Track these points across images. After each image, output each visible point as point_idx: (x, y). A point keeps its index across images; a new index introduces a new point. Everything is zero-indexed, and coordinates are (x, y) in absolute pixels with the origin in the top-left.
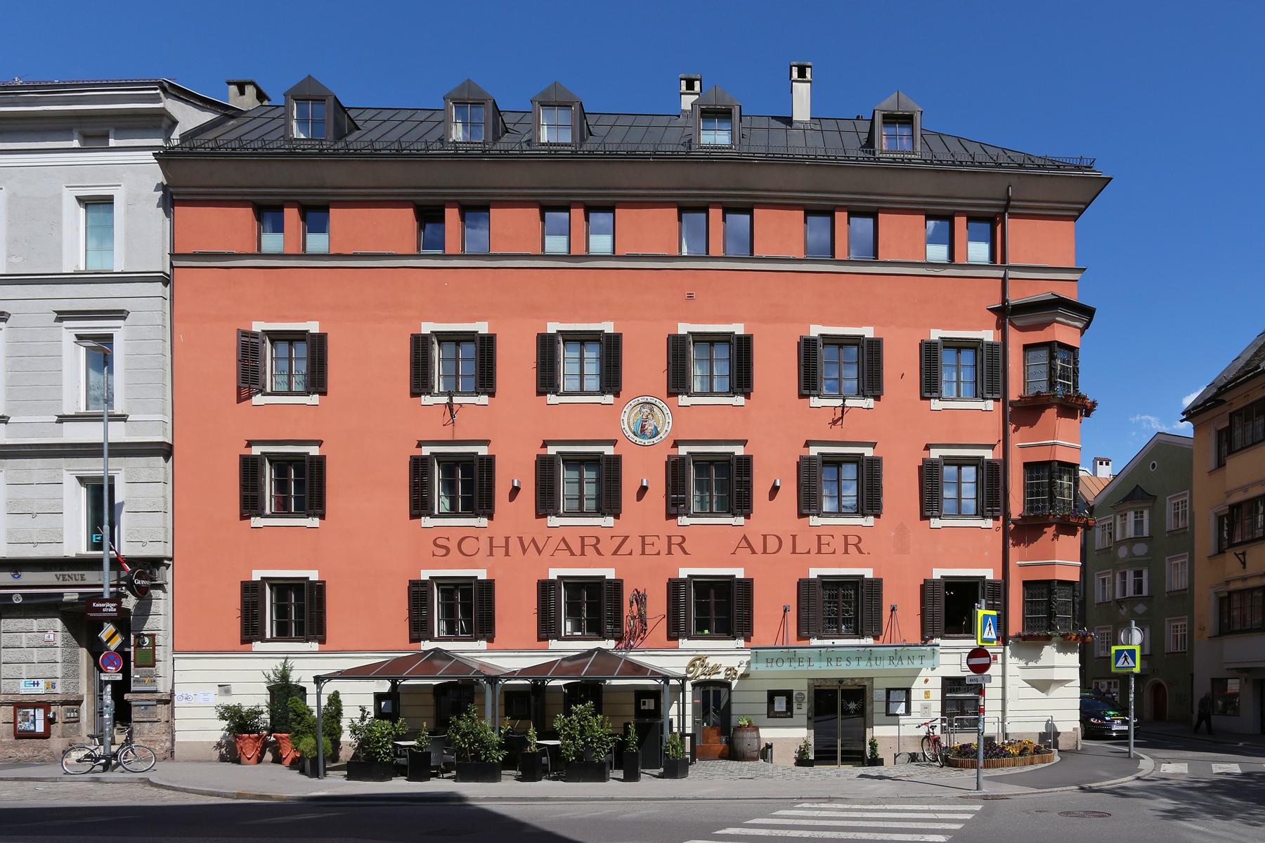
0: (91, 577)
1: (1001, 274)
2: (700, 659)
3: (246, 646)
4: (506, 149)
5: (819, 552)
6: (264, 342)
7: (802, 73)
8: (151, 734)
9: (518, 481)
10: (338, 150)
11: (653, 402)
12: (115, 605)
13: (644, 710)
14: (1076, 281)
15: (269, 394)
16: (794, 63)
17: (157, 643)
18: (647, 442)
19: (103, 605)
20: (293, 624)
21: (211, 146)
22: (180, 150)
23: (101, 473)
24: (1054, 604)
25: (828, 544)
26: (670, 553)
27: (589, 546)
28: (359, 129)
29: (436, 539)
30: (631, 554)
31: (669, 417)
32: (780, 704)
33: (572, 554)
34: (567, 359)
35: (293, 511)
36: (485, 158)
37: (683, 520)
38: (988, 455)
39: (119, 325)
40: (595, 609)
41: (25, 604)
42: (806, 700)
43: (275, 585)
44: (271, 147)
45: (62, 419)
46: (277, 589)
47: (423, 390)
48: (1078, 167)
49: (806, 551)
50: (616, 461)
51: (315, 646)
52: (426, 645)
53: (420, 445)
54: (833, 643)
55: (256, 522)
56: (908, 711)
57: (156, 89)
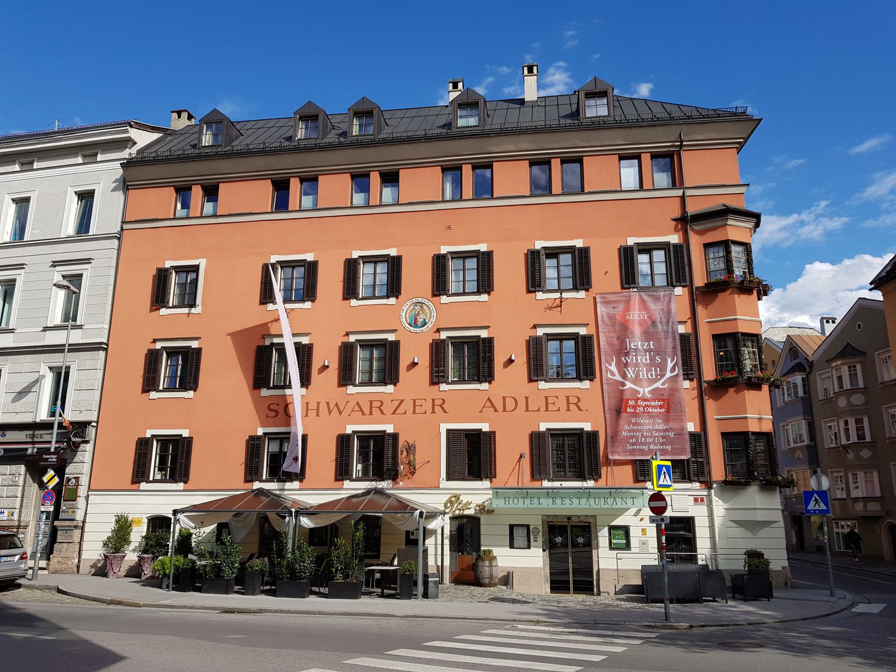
0: (45, 435)
1: (679, 193)
2: (455, 497)
3: (135, 486)
4: (330, 142)
5: (547, 410)
6: (171, 274)
7: (530, 70)
8: (67, 553)
9: (328, 361)
10: (227, 151)
11: (423, 301)
12: (56, 456)
13: (412, 539)
14: (743, 193)
15: (171, 308)
16: (525, 65)
17: (80, 484)
18: (418, 330)
19: (49, 456)
20: (169, 469)
21: (153, 156)
22: (136, 160)
23: (60, 364)
24: (750, 453)
25: (554, 403)
26: (433, 412)
27: (376, 407)
28: (242, 135)
29: (270, 405)
30: (405, 413)
31: (434, 311)
32: (520, 534)
33: (364, 414)
34: (365, 272)
35: (177, 387)
36: (492, 134)
37: (444, 387)
38: (583, 331)
39: (87, 268)
40: (379, 456)
41: (5, 456)
42: (541, 534)
43: (160, 440)
44: (188, 153)
45: (46, 329)
46: (161, 443)
47: (268, 300)
48: (735, 114)
49: (404, 412)
50: (396, 345)
51: (181, 486)
52: (257, 485)
53: (155, 341)
54: (561, 485)
55: (153, 395)
56: (175, 547)
57: (126, 126)
